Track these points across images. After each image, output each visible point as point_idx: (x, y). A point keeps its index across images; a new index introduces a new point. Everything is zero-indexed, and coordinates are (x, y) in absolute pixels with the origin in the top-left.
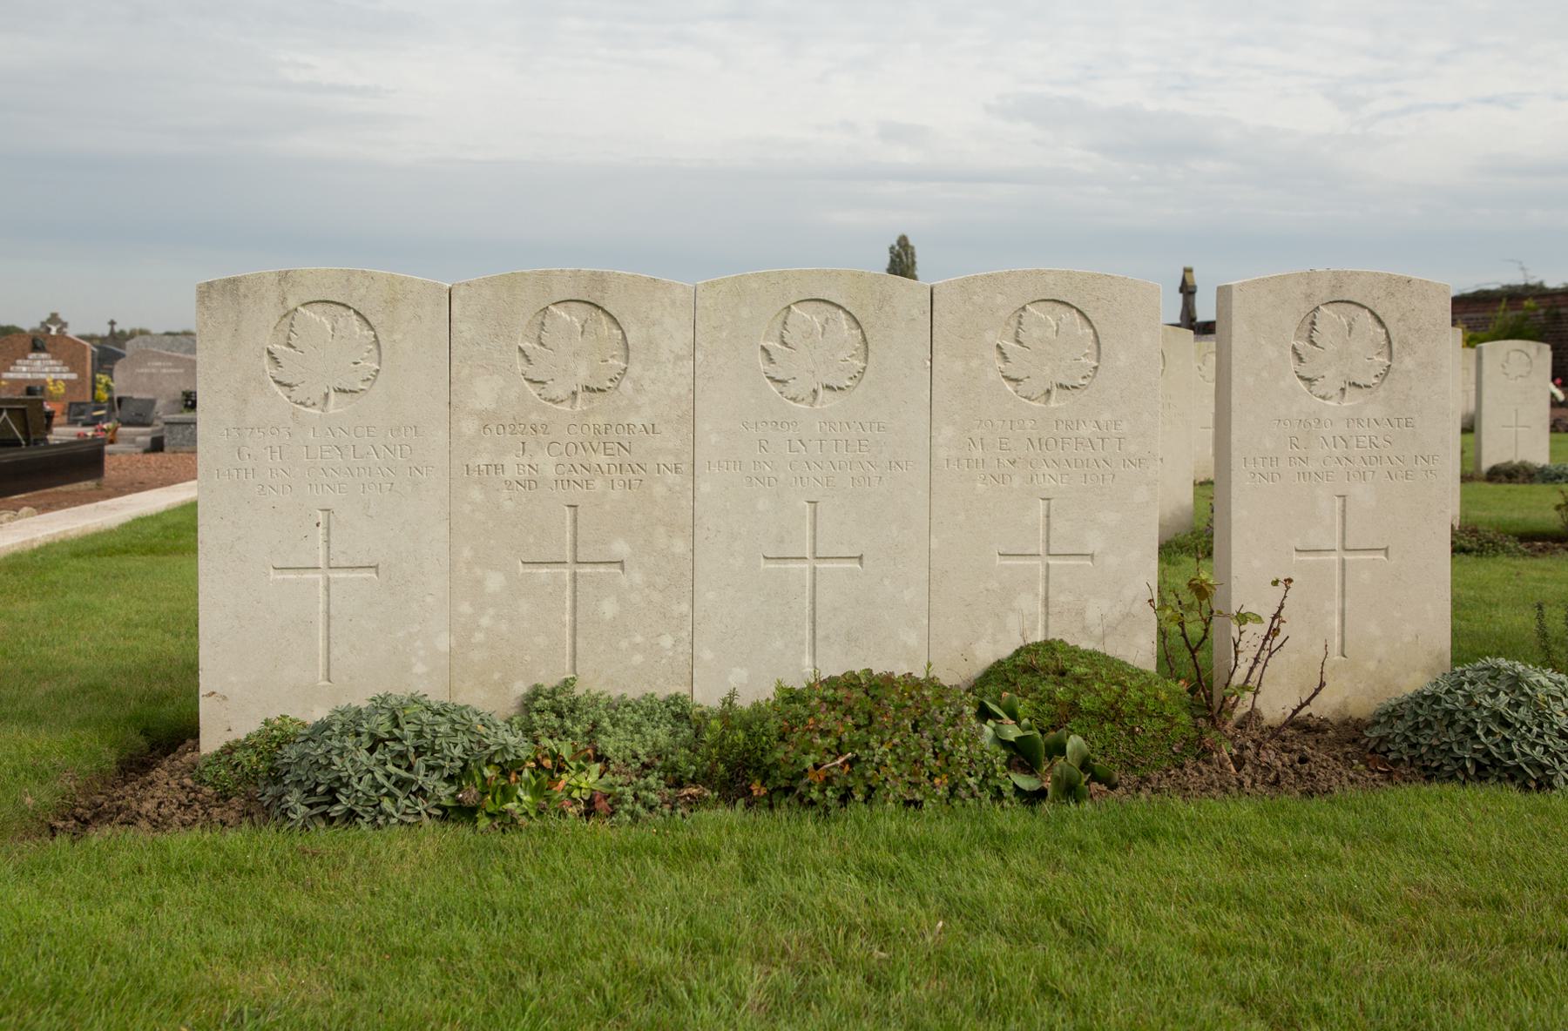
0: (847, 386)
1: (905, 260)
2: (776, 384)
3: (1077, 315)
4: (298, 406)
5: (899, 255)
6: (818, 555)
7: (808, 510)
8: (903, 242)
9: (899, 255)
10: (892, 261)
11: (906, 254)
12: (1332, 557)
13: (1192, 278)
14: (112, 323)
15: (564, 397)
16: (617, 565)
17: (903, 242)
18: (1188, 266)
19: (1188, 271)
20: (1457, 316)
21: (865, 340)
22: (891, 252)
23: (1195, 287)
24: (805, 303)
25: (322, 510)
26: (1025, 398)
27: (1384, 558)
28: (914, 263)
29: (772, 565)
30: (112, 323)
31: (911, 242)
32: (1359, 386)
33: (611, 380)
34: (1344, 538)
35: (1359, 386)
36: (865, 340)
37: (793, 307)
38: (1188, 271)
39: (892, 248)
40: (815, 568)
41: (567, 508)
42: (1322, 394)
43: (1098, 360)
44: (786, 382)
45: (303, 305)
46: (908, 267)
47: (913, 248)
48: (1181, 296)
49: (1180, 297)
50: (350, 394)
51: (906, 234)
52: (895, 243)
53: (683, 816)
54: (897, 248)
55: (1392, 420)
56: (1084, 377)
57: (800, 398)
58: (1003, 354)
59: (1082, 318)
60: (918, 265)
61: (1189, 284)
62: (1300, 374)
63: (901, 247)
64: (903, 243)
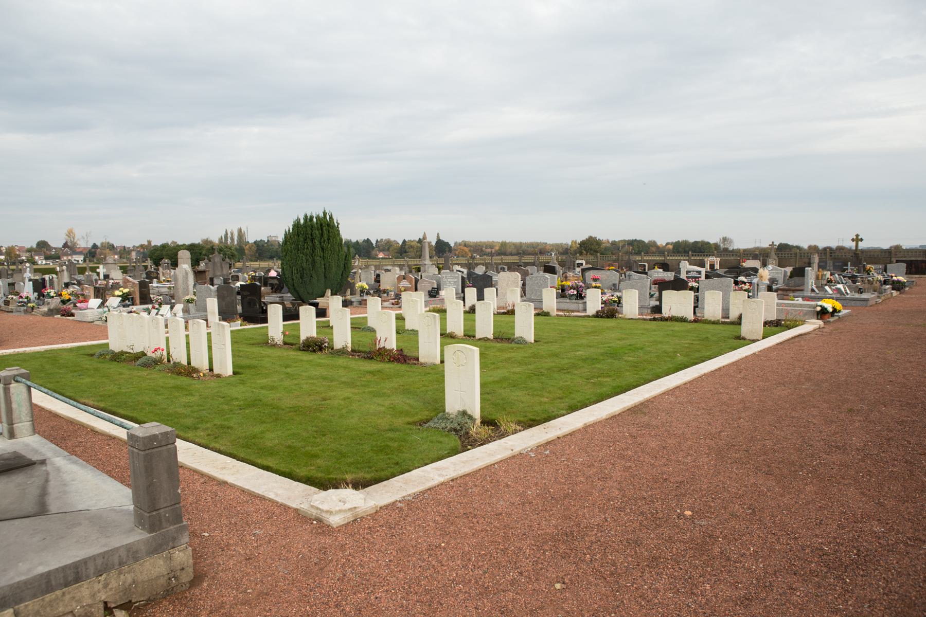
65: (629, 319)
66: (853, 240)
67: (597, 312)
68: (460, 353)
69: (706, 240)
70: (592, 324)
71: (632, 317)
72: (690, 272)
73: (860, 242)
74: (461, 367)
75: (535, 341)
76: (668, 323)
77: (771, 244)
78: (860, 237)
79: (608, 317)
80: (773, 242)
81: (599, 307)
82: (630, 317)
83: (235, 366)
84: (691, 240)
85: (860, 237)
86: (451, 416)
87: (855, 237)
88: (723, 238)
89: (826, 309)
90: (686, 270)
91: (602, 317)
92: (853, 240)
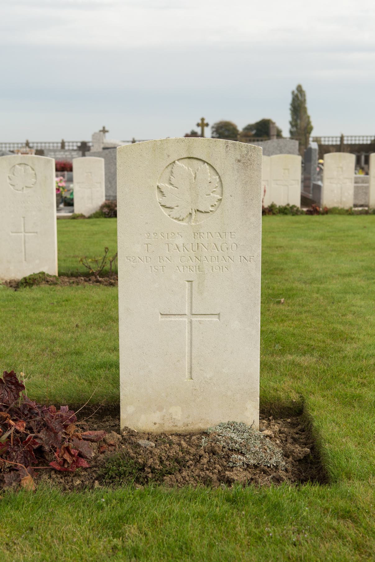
0: (211, 211)
2: (166, 209)
3: (208, 167)
4: (173, 220)
6: (193, 313)
7: (187, 286)
8: (299, 89)
11: (301, 95)
12: (184, 319)
15: (184, 216)
16: (217, 316)
17: (299, 89)
21: (221, 181)
24: (183, 160)
25: (187, 281)
26: (176, 219)
27: (218, 320)
28: (305, 100)
32: (201, 212)
33: (212, 206)
35: (201, 212)
36: (221, 181)
37: (176, 162)
39: (293, 93)
41: (187, 282)
42: (178, 216)
43: (222, 194)
44: (172, 208)
45: (178, 160)
50: (205, 214)
55: (222, 234)
56: (212, 206)
57: (181, 218)
58: (162, 192)
59: (211, 168)
62: (162, 204)
66: (198, 125)
77: (205, 122)
80: (203, 120)
92: (198, 125)
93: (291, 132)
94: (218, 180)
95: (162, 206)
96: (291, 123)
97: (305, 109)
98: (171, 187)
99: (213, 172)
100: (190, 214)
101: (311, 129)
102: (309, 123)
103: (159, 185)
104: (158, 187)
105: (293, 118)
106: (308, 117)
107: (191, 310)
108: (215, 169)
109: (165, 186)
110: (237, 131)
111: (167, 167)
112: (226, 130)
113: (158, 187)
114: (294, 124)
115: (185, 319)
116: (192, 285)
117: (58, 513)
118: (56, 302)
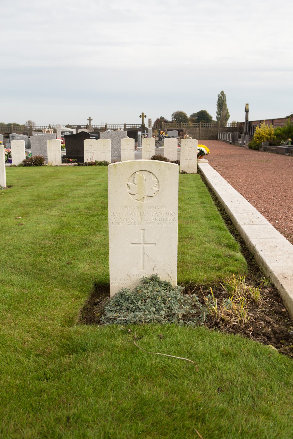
1: (223, 99)
5: (221, 97)
8: (222, 93)
9: (221, 97)
10: (219, 99)
11: (223, 97)
13: (248, 107)
14: (90, 120)
17: (222, 93)
18: (247, 103)
19: (247, 105)
20: (163, 130)
22: (218, 96)
23: (248, 110)
28: (225, 100)
29: (133, 246)
30: (143, 116)
31: (225, 93)
34: (144, 240)
38: (247, 105)
39: (219, 95)
40: (144, 247)
42: (137, 199)
46: (224, 101)
47: (225, 95)
48: (245, 113)
49: (245, 113)
51: (223, 91)
52: (220, 93)
53: (189, 436)
54: (220, 95)
60: (227, 101)
61: (247, 109)
63: (222, 95)
64: (222, 93)
65: (55, 166)
67: (24, 161)
68: (145, 175)
69: (17, 122)
70: (36, 170)
71: (57, 165)
72: (64, 132)
73: (144, 118)
74: (147, 201)
75: (7, 186)
76: (93, 167)
78: (144, 115)
79: (36, 165)
80: (90, 118)
81: (23, 157)
82: (56, 165)
83: (26, 135)
84: (6, 123)
85: (144, 115)
86: (128, 293)
87: (141, 115)
88: (28, 121)
89: (203, 152)
90: (61, 131)
91: (30, 165)
93: (217, 118)
94: (157, 181)
95: (130, 194)
96: (217, 113)
97: (225, 105)
98: (134, 184)
99: (154, 177)
100: (144, 197)
101: (229, 116)
102: (227, 113)
103: (128, 183)
104: (128, 185)
105: (218, 110)
106: (227, 109)
107: (144, 241)
108: (155, 175)
109: (131, 184)
110: (187, 117)
111: (131, 176)
112: (180, 116)
113: (128, 185)
114: (219, 113)
115: (141, 246)
116: (144, 231)
117: (41, 409)
118: (6, 407)
